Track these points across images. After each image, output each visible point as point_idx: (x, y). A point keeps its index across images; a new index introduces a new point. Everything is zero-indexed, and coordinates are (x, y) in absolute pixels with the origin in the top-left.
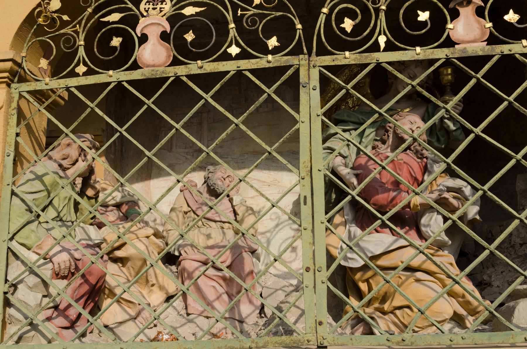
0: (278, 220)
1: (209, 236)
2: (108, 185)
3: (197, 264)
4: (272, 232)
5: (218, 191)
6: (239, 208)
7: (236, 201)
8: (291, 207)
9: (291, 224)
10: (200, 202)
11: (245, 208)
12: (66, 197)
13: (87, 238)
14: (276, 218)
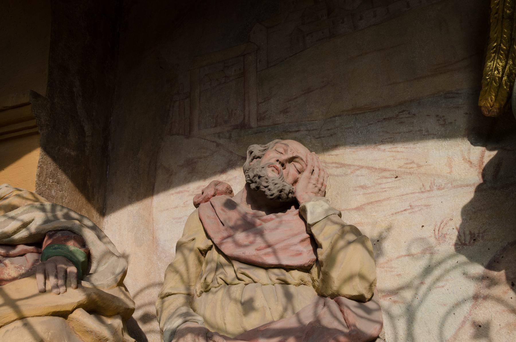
0: (428, 256)
1: (248, 306)
4: (417, 288)
5: (268, 193)
6: (322, 230)
7: (312, 213)
8: (458, 221)
9: (465, 263)
10: (231, 224)
11: (337, 228)
14: (424, 252)
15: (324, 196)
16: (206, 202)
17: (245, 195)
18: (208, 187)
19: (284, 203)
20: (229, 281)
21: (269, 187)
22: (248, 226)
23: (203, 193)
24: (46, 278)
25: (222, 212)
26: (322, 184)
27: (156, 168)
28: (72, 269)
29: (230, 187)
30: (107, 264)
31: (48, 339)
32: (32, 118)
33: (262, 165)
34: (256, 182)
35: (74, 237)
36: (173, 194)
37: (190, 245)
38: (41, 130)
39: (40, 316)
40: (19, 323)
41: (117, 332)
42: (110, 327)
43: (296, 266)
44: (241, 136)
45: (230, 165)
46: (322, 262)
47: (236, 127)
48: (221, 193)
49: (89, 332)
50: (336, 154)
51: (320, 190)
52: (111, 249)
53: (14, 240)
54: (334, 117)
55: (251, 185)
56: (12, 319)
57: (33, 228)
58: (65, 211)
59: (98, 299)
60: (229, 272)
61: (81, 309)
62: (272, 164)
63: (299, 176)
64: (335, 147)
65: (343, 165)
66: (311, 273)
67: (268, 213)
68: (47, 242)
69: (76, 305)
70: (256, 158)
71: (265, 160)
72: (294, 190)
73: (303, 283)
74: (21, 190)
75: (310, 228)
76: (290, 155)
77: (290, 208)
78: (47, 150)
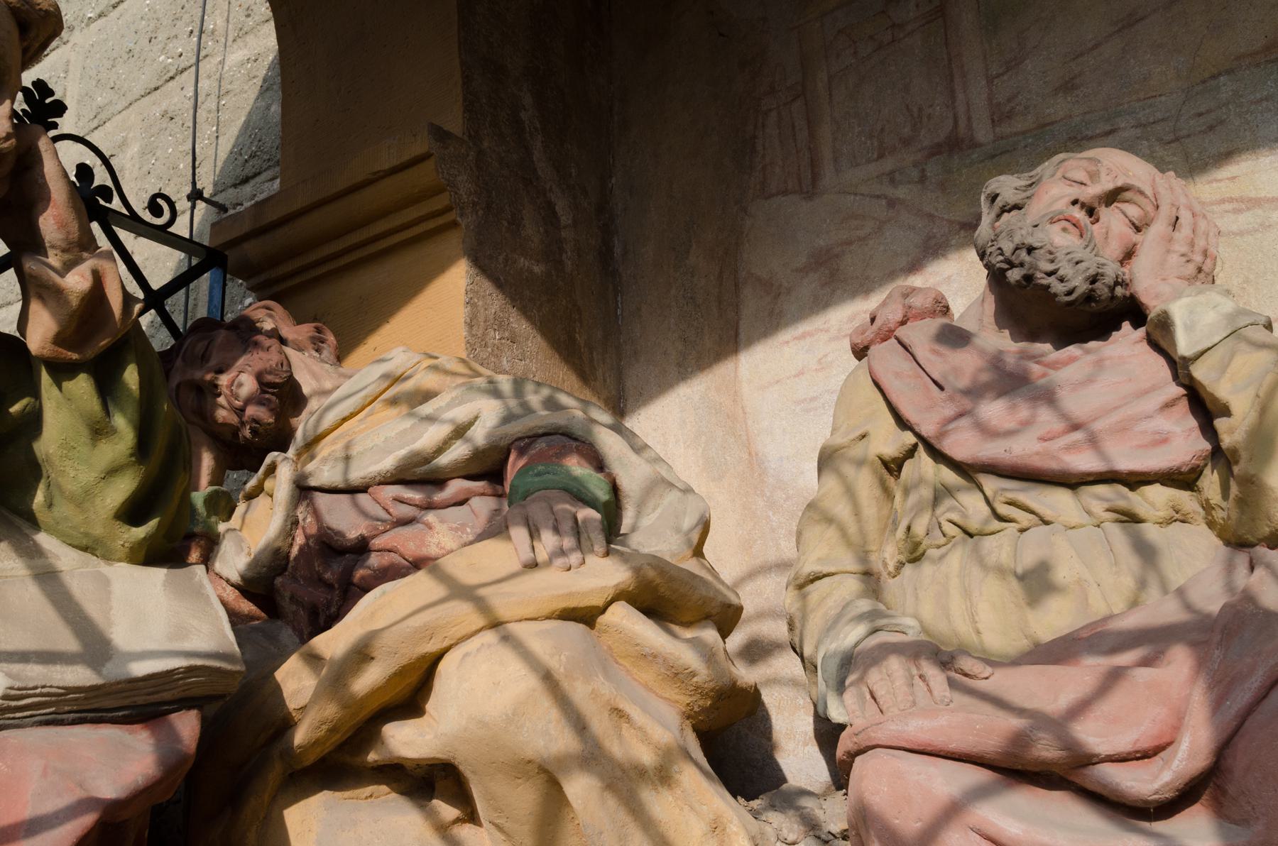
1: (1037, 583)
3: (951, 780)
5: (1058, 288)
6: (1223, 368)
10: (964, 382)
13: (70, 644)
15: (1213, 282)
16: (884, 340)
17: (990, 306)
18: (884, 304)
19: (1102, 313)
20: (973, 525)
21: (1061, 273)
22: (1009, 381)
23: (873, 320)
24: (534, 534)
25: (933, 357)
26: (1205, 253)
27: (736, 285)
28: (587, 514)
29: (943, 297)
30: (659, 510)
31: (562, 670)
32: (437, 191)
33: (1030, 220)
34: (1022, 265)
35: (577, 447)
36: (787, 342)
37: (857, 451)
38: (462, 215)
39: (535, 619)
40: (490, 637)
41: (714, 655)
42: (696, 644)
43: (1156, 474)
44: (949, 172)
45: (933, 249)
46: (1234, 451)
47: (936, 150)
48: (922, 315)
49: (649, 657)
50: (1229, 175)
51: (1200, 270)
52: (664, 473)
53: (438, 469)
54: (1214, 77)
55: (1009, 274)
56: (474, 628)
57: (479, 435)
58: (545, 392)
59: (658, 581)
60: (972, 506)
61: (623, 603)
62: (1061, 213)
63: (1137, 238)
64: (1226, 156)
65: (1255, 203)
66: (1199, 491)
67: (1061, 343)
68: (514, 465)
69: (609, 594)
70: (1009, 211)
71: (1035, 210)
72: (1127, 277)
73: (1179, 517)
74: (436, 358)
75: (1187, 368)
76: (1106, 184)
77: (1118, 328)
78: (481, 264)
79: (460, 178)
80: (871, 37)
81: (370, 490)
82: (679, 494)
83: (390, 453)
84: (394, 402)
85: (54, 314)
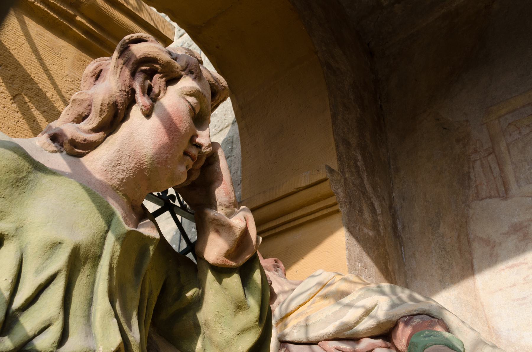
2: (351, 282)
12: (55, 245)
27: (469, 242)
53: (357, 333)
78: (351, 231)
79: (339, 190)
80: (528, 126)
81: (319, 343)
82: (491, 348)
83: (330, 323)
84: (325, 297)
85: (226, 240)
